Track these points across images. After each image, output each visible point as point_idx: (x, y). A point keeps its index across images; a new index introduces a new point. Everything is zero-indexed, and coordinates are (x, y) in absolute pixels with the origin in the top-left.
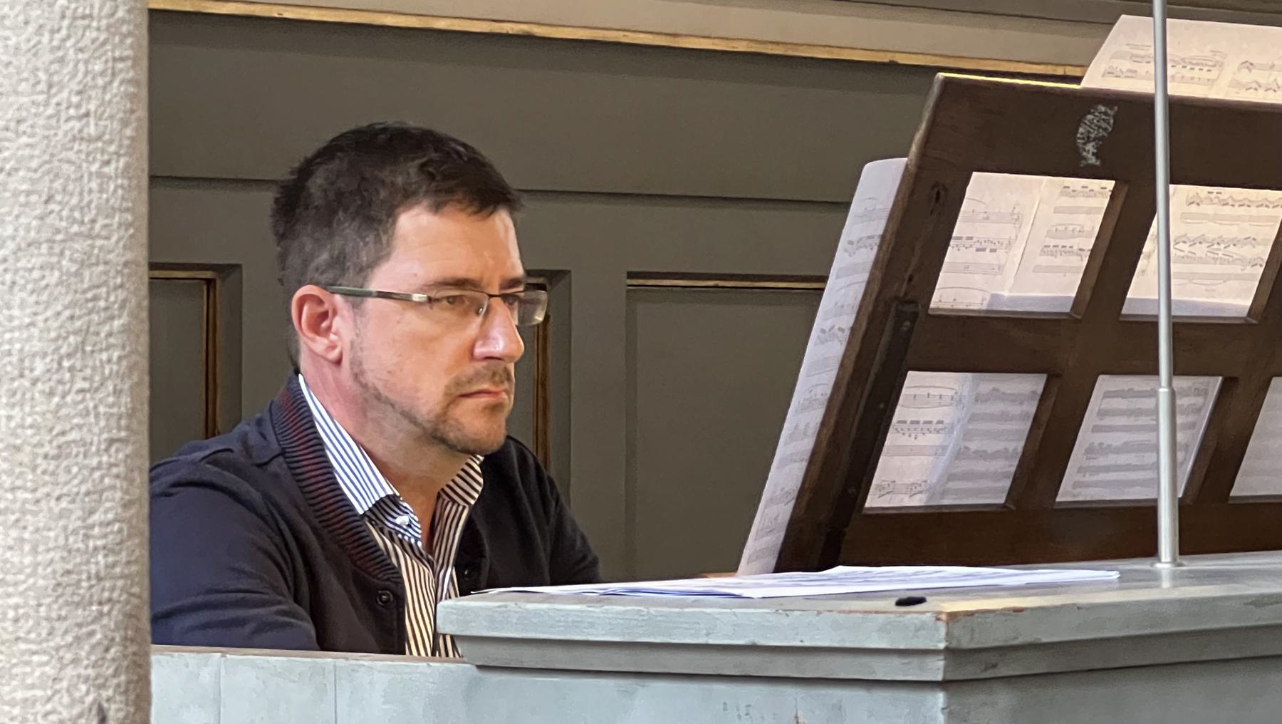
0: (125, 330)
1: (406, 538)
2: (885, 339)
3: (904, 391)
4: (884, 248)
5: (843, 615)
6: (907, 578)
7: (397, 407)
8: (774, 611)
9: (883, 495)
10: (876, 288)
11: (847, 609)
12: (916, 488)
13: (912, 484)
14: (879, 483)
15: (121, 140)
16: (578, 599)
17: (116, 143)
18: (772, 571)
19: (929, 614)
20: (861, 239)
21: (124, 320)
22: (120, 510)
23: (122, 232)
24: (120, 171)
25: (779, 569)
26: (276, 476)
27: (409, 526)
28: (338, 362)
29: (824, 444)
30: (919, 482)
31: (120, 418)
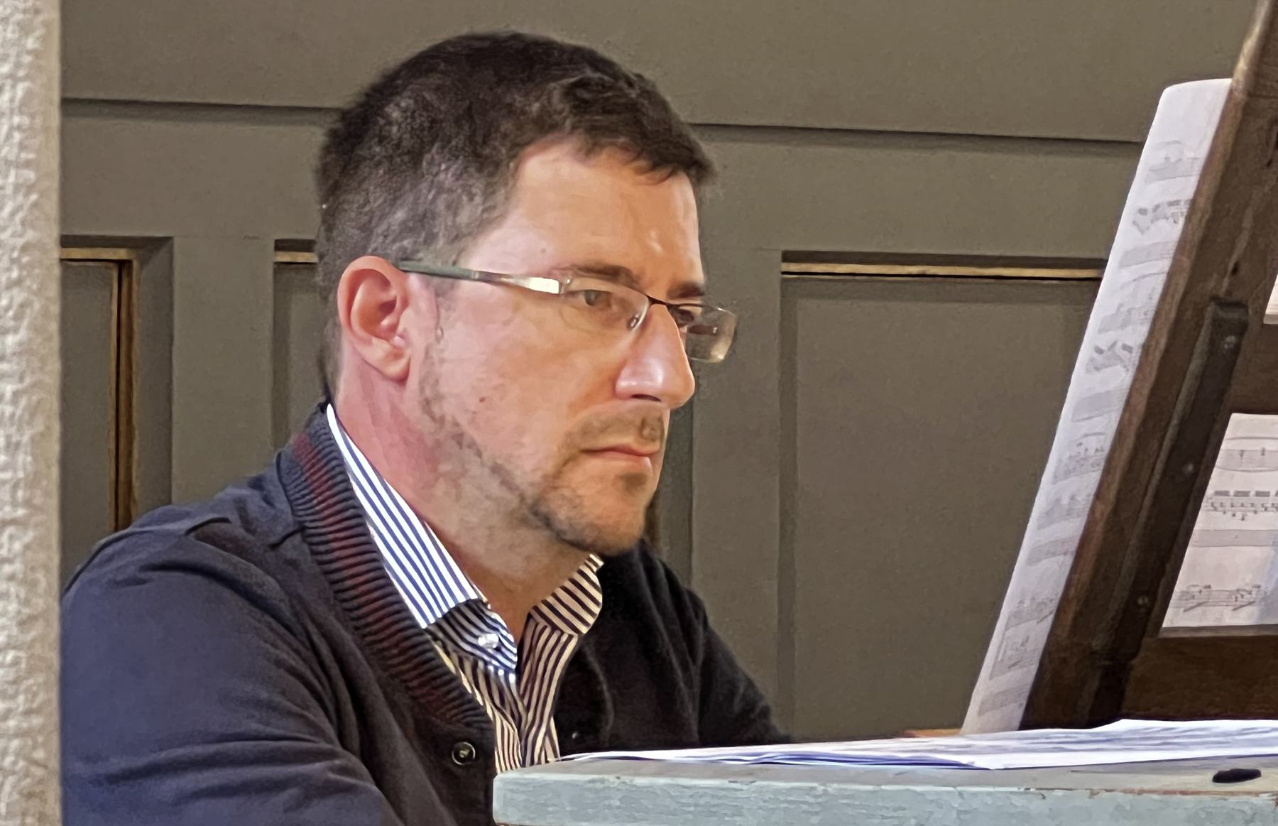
0: (24, 351)
1: (491, 668)
2: (1195, 365)
3: (1225, 446)
4: (1195, 220)
5: (1130, 796)
6: (1229, 739)
7: (485, 456)
8: (1022, 790)
9: (1192, 608)
10: (1182, 282)
11: (1137, 787)
12: (1242, 596)
13: (1238, 590)
14: (1185, 589)
15: (18, 55)
16: (713, 769)
17: (12, 59)
18: (1017, 723)
19: (1265, 796)
20: (1157, 207)
21: (23, 334)
22: (15, 631)
23: (20, 198)
24: (17, 103)
25: (1024, 726)
26: (293, 563)
27: (498, 650)
28: (402, 380)
29: (1099, 528)
30: (1247, 588)
31: (15, 487)
